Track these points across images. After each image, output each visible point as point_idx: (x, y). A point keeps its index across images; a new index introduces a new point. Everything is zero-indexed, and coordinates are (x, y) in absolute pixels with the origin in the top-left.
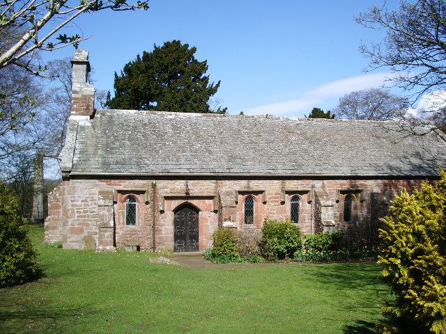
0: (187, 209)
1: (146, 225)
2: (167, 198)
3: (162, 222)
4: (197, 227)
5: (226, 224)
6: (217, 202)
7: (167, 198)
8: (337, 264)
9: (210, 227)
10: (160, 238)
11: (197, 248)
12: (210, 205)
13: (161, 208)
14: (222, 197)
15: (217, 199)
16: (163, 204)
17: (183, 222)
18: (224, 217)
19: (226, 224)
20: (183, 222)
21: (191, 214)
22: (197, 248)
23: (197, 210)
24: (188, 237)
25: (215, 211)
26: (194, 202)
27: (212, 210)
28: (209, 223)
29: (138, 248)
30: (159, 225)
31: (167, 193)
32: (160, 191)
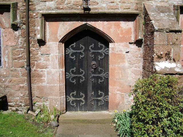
0: (88, 39)
1: (16, 66)
2: (49, 17)
3: (42, 61)
4: (107, 69)
5: (161, 66)
6: (142, 26)
7: (49, 17)
8: (47, 26)
9: (129, 71)
10: (41, 89)
11: (106, 106)
12: (128, 31)
13: (39, 37)
14: (151, 14)
15: (141, 20)
16: (44, 28)
17: (81, 61)
18: (158, 50)
19: (161, 66)
20: (81, 61)
21: (96, 48)
22: (106, 106)
23: (105, 41)
24: (90, 87)
25: (138, 43)
26: (100, 25)
27: (133, 40)
28: (127, 64)
29: (177, 40)
30: (38, 66)
31: (50, 8)
32: (38, 7)
